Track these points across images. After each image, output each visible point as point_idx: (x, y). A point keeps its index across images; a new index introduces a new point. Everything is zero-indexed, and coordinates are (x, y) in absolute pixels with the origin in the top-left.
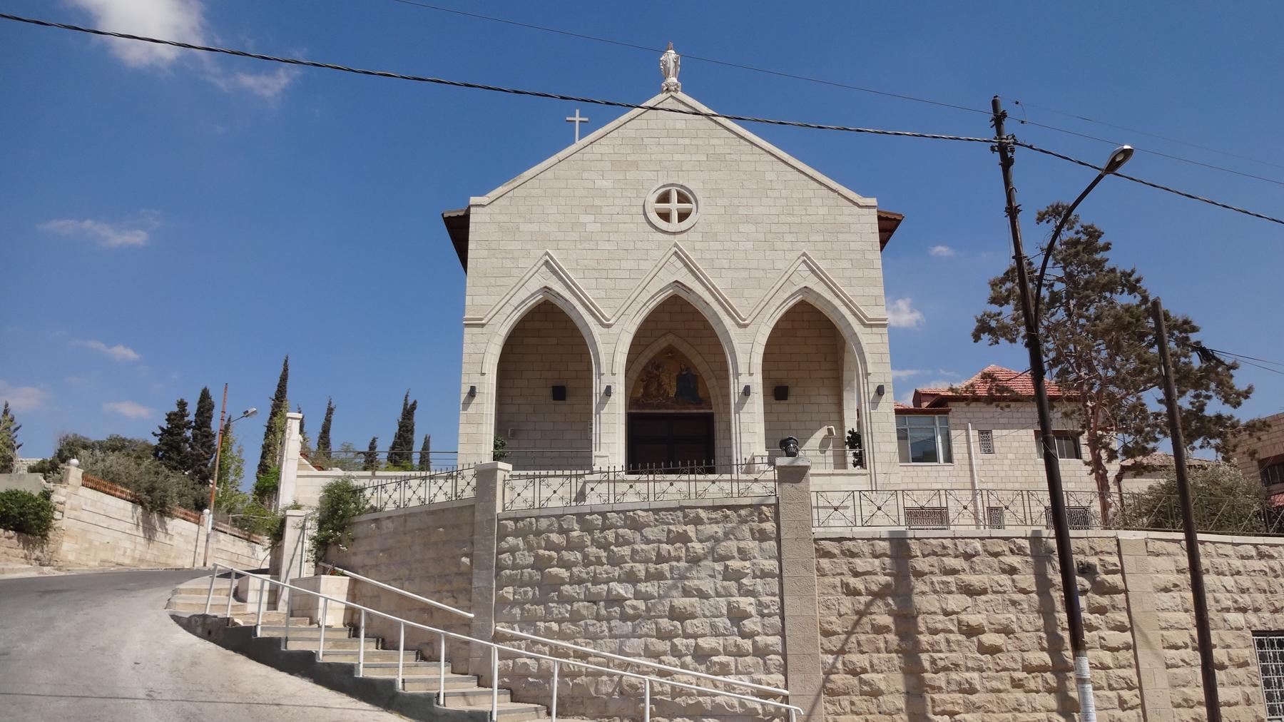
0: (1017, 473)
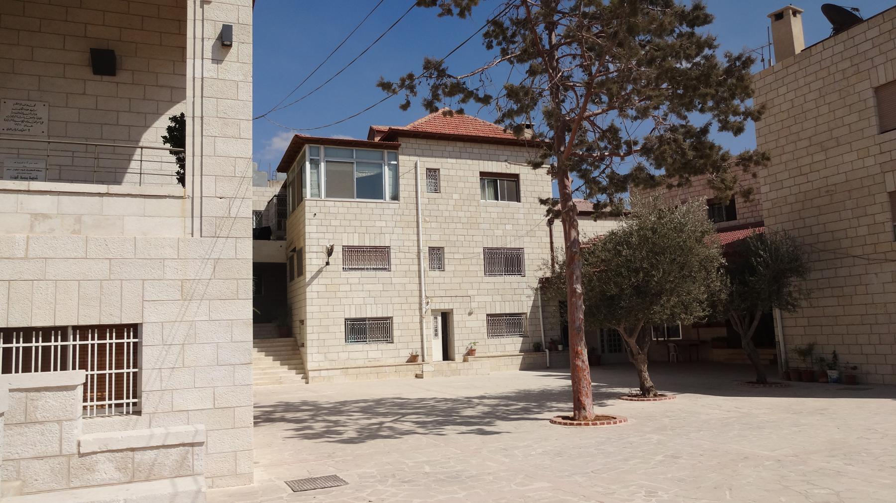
0: (461, 214)
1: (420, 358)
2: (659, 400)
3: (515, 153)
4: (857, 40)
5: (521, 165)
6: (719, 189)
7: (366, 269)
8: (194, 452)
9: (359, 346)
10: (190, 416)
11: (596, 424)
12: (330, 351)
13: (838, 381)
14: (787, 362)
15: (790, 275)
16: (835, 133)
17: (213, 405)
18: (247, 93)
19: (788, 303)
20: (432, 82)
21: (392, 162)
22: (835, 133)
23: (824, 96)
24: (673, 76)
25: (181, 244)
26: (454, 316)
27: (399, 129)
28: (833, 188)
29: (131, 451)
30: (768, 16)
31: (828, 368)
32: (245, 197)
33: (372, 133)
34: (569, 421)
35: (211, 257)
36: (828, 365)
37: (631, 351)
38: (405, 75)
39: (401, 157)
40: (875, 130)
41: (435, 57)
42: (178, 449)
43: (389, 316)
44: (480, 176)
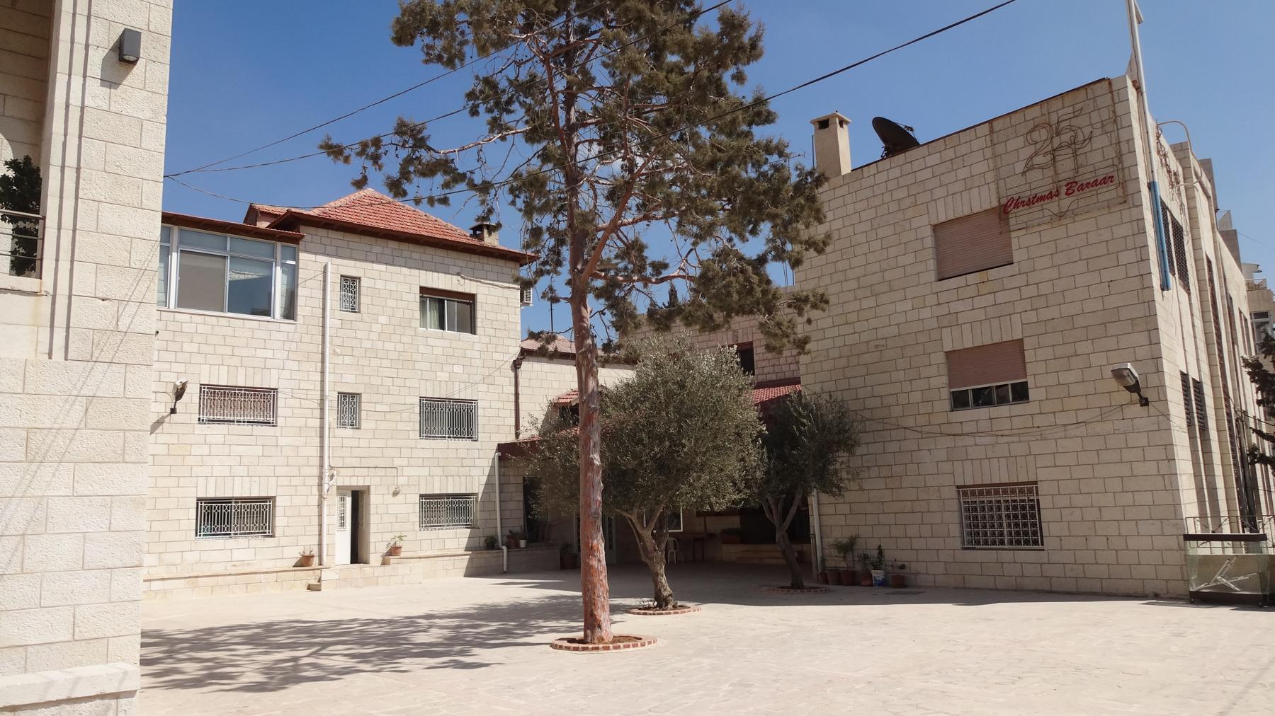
0: (389, 346)
1: (316, 561)
2: (682, 613)
3: (471, 264)
4: (916, 166)
5: (480, 282)
6: (775, 335)
7: (237, 422)
8: (119, 708)
9: (219, 542)
10: (28, 654)
11: (619, 647)
12: (168, 550)
13: (883, 584)
14: (823, 560)
15: (835, 449)
16: (888, 275)
17: (71, 636)
18: (156, 138)
19: (833, 485)
20: (404, 153)
21: (288, 262)
22: (888, 275)
23: (876, 229)
24: (729, 186)
25: (29, 368)
26: (371, 496)
27: (309, 215)
28: (883, 342)
29: (11, 711)
30: (811, 122)
31: (873, 568)
32: (144, 301)
33: (253, 214)
34: (581, 646)
35: (83, 393)
36: (872, 563)
37: (645, 548)
38: (369, 137)
39: (302, 256)
40: (932, 276)
41: (413, 119)
42: (92, 703)
43: (270, 495)
44: (420, 293)
